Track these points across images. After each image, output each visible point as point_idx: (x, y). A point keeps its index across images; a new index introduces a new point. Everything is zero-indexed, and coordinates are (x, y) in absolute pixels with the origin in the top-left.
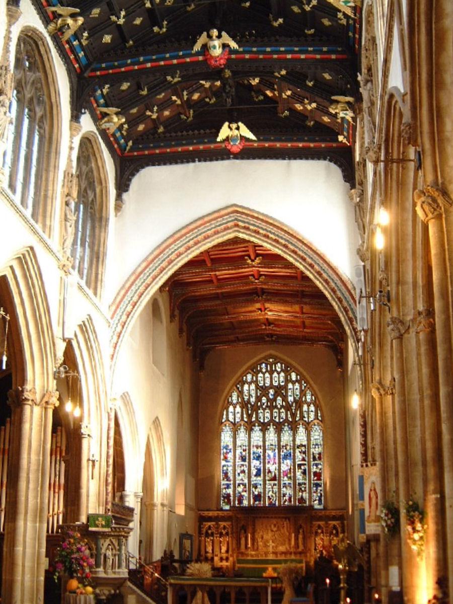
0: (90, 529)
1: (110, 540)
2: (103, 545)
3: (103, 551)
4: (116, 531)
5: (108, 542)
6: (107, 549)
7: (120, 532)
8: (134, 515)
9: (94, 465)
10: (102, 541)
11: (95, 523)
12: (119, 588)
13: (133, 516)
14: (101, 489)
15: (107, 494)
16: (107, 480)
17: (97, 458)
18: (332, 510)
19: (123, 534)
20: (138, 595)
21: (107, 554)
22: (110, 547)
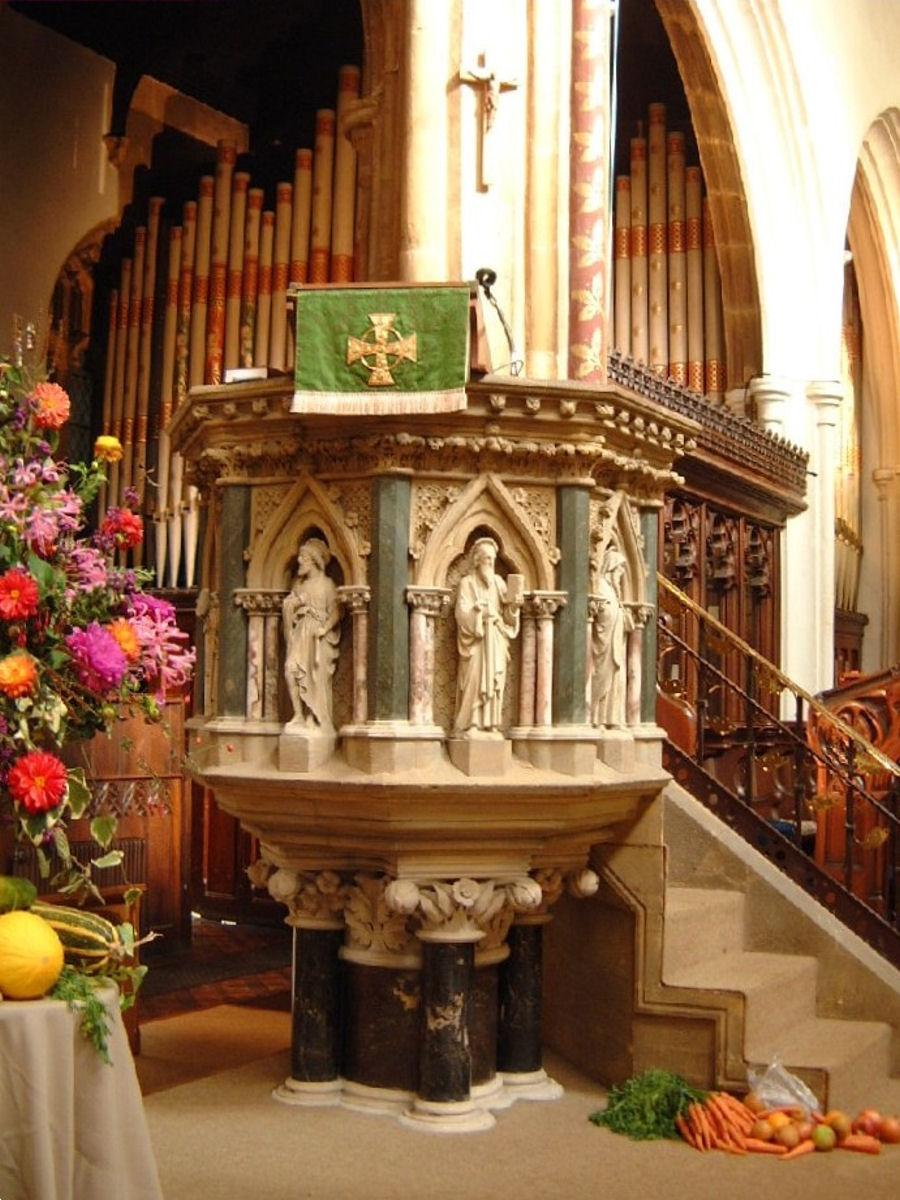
0: (305, 402)
1: (488, 492)
2: (425, 531)
3: (429, 579)
4: (529, 424)
5: (466, 507)
6: (463, 561)
7: (564, 428)
8: (809, 478)
9: (486, 108)
10: (414, 506)
11: (339, 350)
12: (597, 860)
13: (802, 485)
14: (541, 247)
15: (578, 279)
16: (575, 202)
17: (505, 67)
18: (173, 778)
19: (593, 446)
20: (761, 892)
21: (465, 606)
22: (489, 549)
